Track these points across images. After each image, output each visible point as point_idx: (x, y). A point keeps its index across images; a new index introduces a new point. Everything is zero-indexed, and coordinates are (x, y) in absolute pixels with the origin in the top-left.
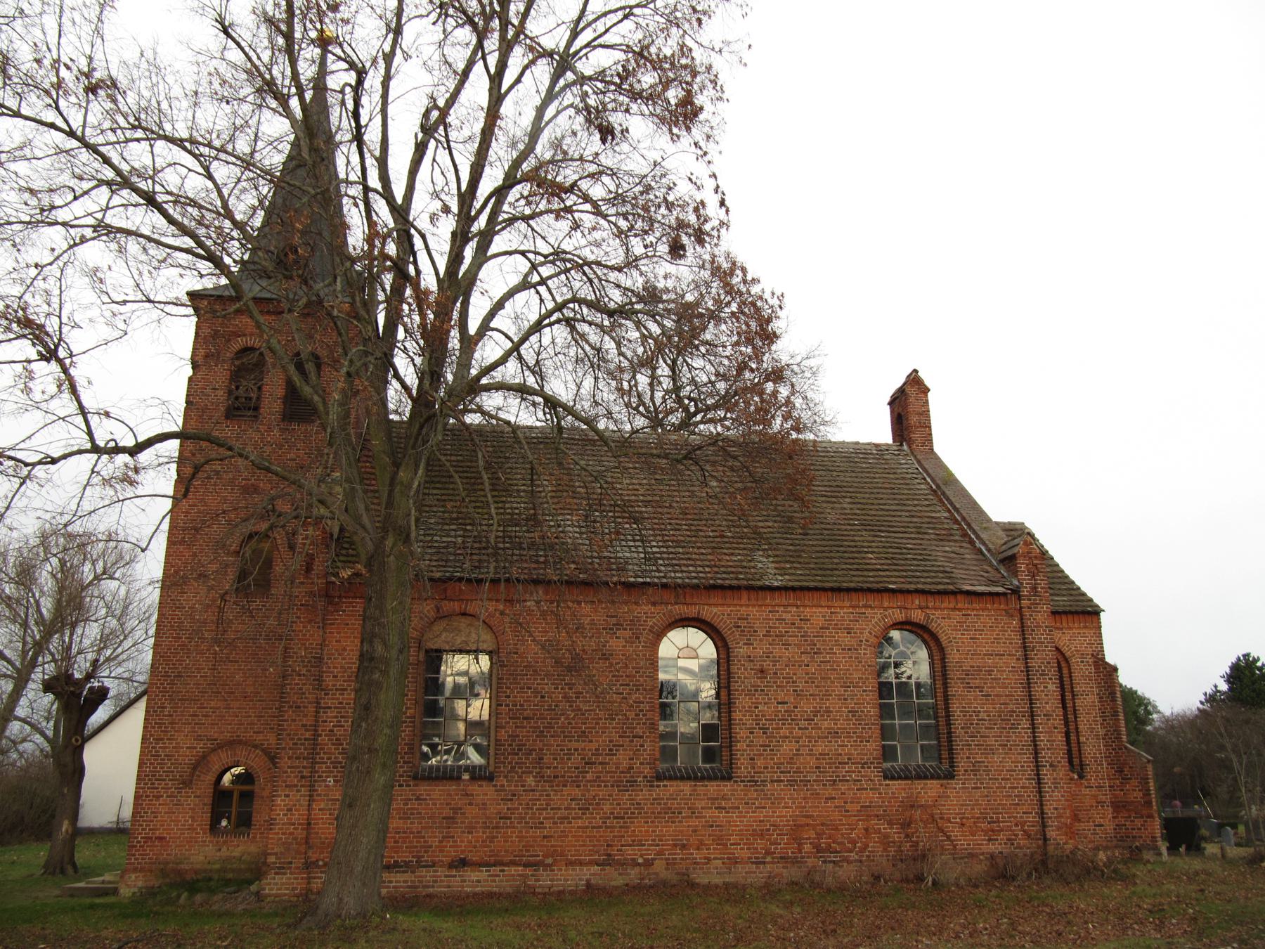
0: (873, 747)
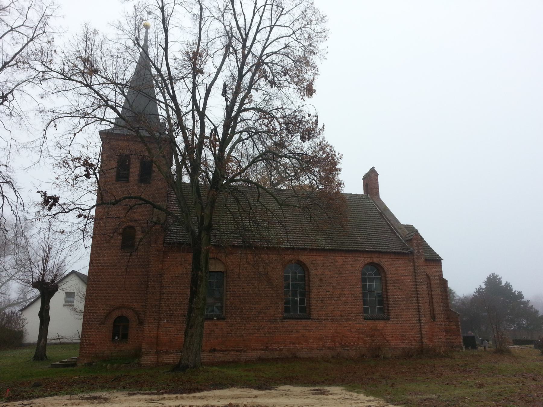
0: (361, 308)
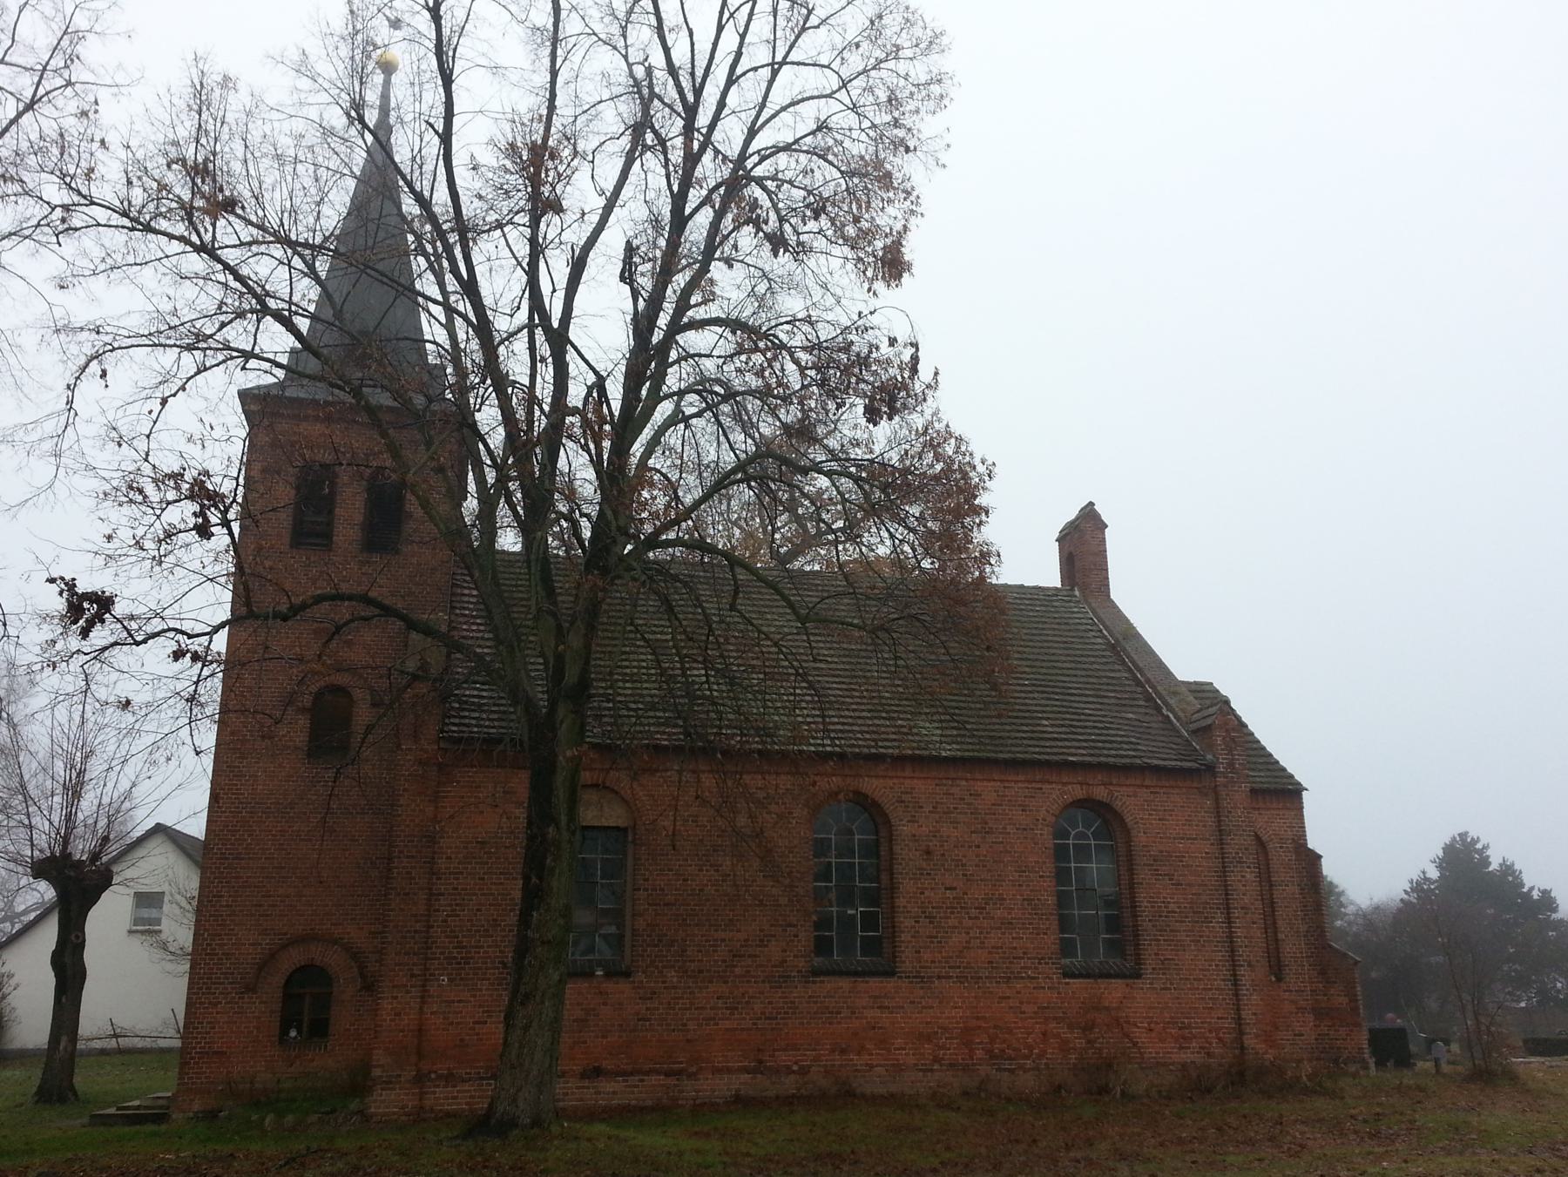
0: (1051, 939)
